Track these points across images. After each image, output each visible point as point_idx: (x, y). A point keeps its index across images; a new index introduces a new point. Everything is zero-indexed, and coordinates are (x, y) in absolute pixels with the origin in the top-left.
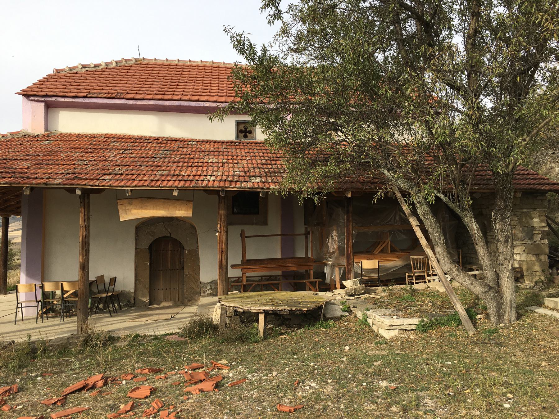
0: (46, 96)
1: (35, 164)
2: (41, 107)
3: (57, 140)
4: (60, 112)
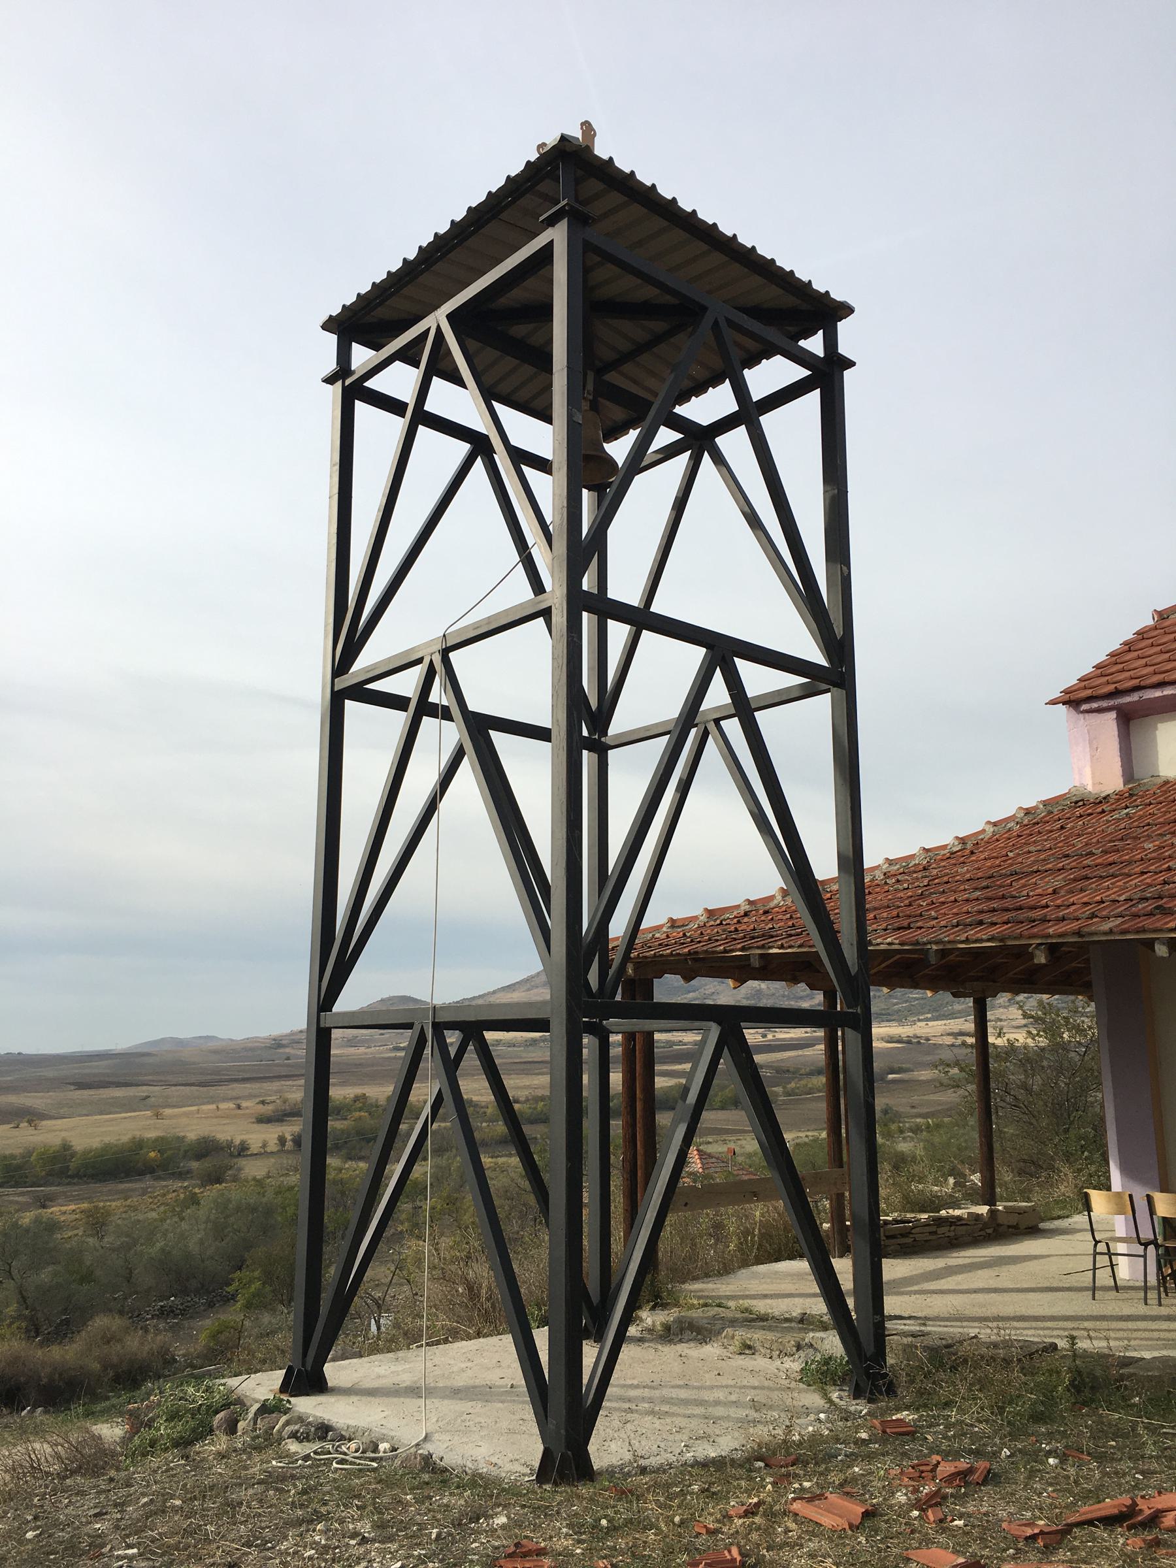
0: (1117, 693)
1: (1075, 880)
2: (1108, 723)
3: (1150, 804)
4: (1160, 726)
